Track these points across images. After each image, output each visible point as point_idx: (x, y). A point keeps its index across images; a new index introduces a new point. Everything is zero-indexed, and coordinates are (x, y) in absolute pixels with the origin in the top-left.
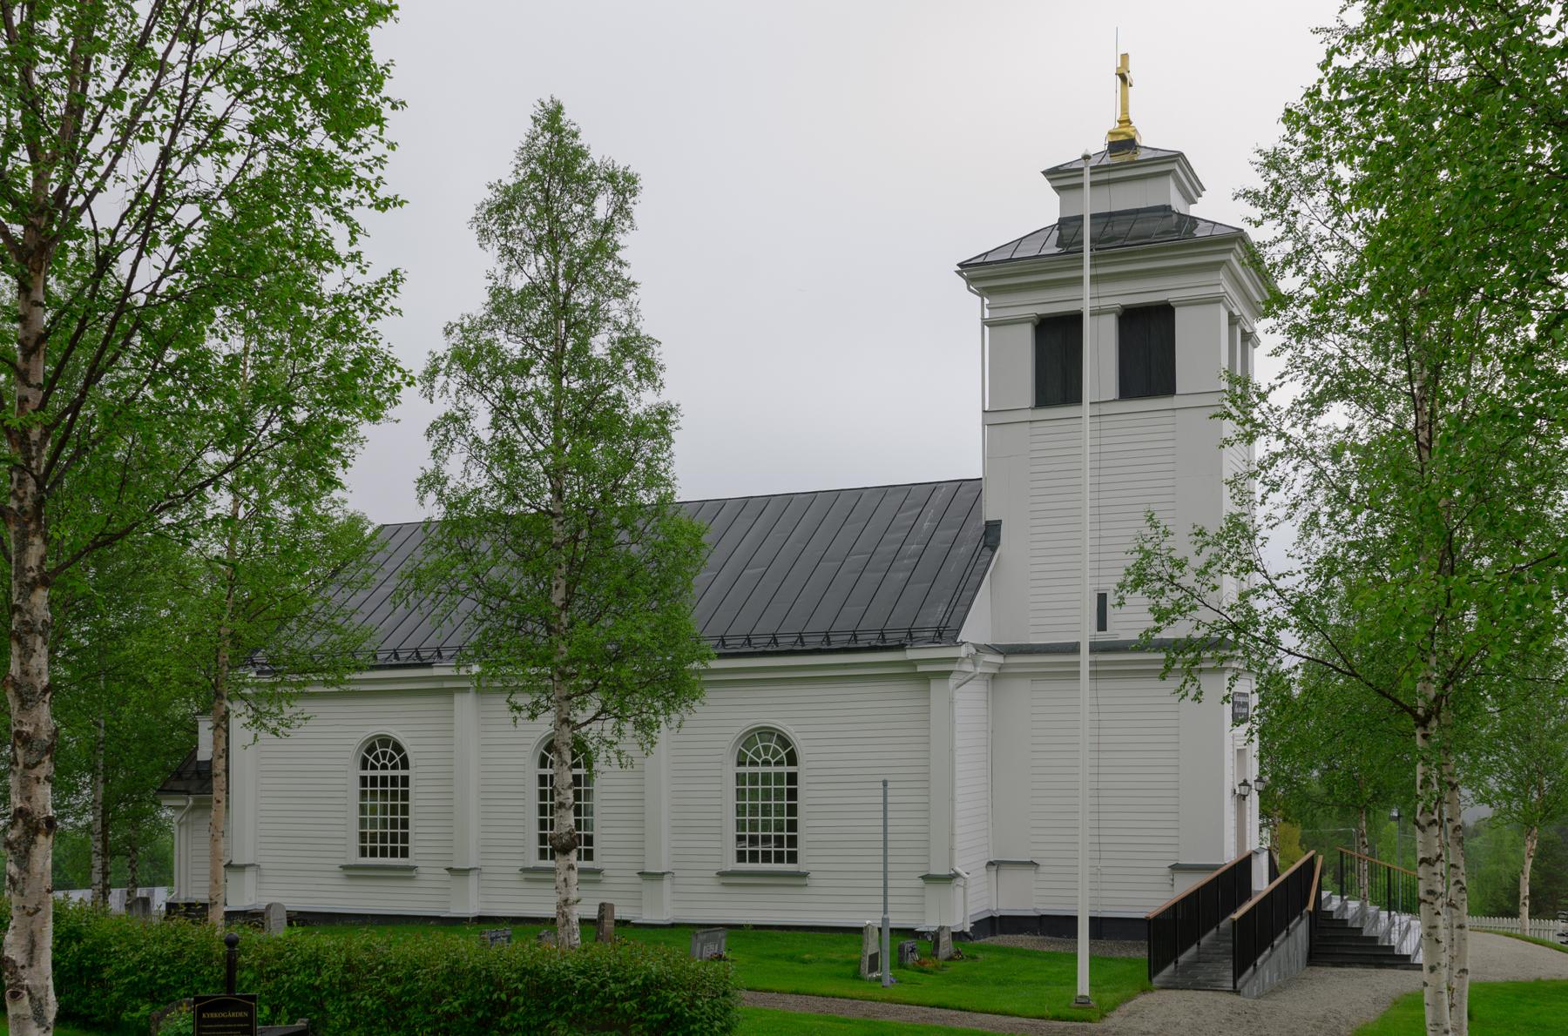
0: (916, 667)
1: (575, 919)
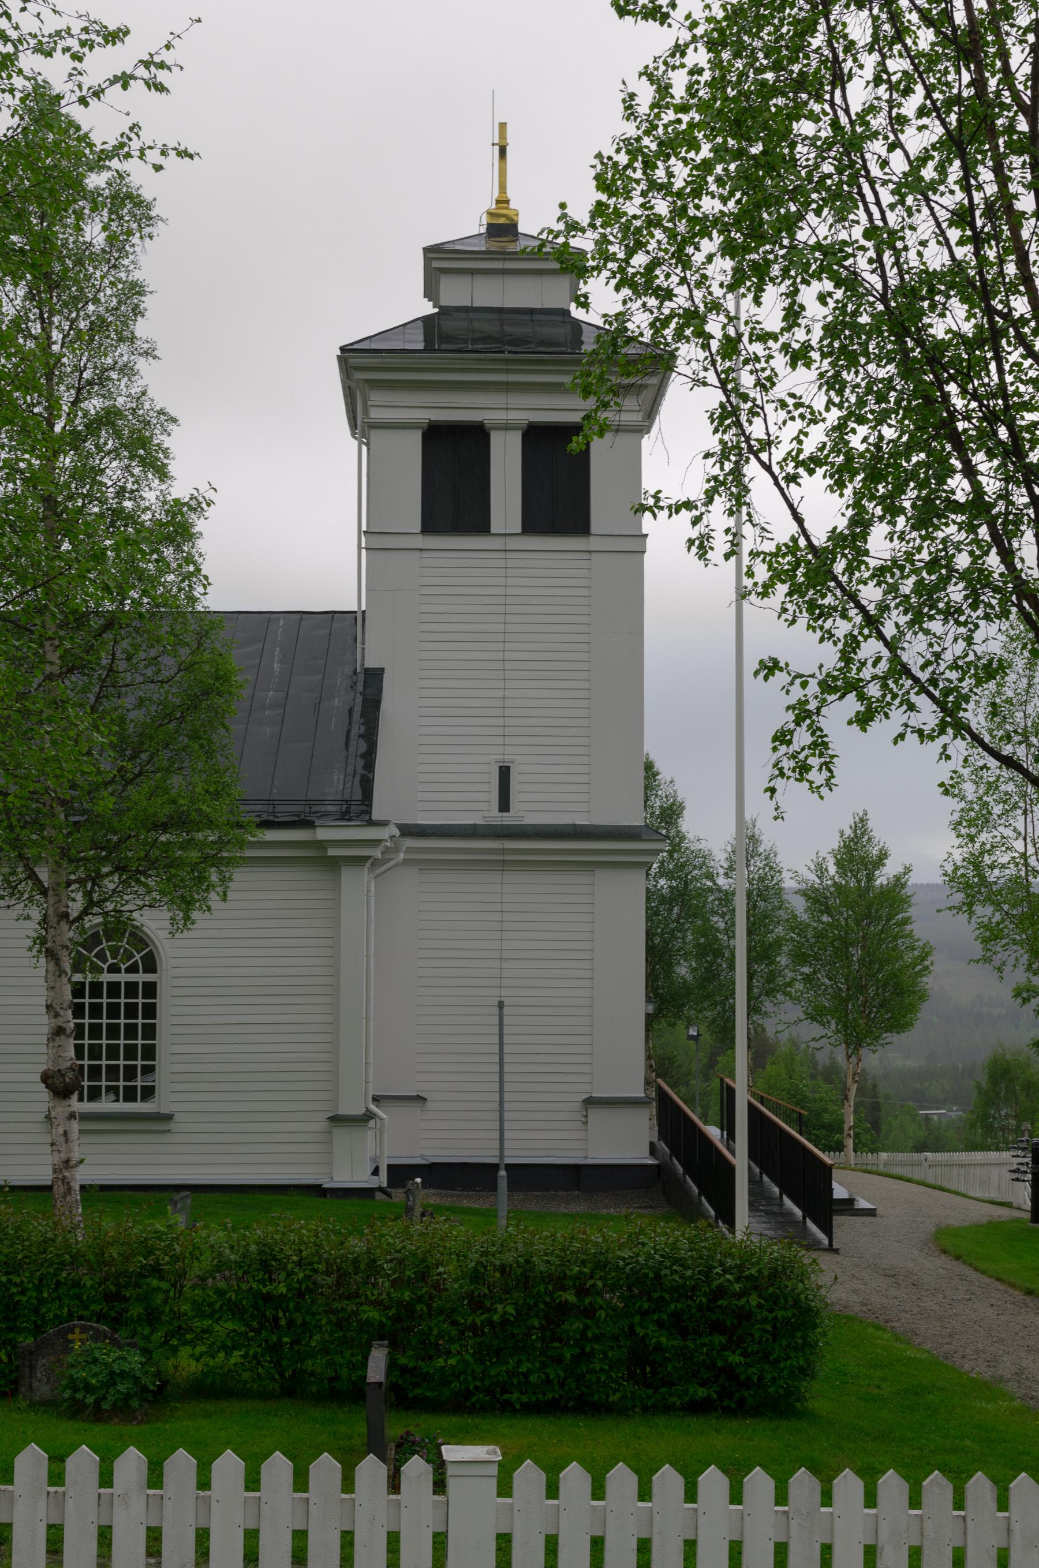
0: (325, 849)
1: (77, 1187)
